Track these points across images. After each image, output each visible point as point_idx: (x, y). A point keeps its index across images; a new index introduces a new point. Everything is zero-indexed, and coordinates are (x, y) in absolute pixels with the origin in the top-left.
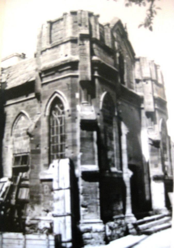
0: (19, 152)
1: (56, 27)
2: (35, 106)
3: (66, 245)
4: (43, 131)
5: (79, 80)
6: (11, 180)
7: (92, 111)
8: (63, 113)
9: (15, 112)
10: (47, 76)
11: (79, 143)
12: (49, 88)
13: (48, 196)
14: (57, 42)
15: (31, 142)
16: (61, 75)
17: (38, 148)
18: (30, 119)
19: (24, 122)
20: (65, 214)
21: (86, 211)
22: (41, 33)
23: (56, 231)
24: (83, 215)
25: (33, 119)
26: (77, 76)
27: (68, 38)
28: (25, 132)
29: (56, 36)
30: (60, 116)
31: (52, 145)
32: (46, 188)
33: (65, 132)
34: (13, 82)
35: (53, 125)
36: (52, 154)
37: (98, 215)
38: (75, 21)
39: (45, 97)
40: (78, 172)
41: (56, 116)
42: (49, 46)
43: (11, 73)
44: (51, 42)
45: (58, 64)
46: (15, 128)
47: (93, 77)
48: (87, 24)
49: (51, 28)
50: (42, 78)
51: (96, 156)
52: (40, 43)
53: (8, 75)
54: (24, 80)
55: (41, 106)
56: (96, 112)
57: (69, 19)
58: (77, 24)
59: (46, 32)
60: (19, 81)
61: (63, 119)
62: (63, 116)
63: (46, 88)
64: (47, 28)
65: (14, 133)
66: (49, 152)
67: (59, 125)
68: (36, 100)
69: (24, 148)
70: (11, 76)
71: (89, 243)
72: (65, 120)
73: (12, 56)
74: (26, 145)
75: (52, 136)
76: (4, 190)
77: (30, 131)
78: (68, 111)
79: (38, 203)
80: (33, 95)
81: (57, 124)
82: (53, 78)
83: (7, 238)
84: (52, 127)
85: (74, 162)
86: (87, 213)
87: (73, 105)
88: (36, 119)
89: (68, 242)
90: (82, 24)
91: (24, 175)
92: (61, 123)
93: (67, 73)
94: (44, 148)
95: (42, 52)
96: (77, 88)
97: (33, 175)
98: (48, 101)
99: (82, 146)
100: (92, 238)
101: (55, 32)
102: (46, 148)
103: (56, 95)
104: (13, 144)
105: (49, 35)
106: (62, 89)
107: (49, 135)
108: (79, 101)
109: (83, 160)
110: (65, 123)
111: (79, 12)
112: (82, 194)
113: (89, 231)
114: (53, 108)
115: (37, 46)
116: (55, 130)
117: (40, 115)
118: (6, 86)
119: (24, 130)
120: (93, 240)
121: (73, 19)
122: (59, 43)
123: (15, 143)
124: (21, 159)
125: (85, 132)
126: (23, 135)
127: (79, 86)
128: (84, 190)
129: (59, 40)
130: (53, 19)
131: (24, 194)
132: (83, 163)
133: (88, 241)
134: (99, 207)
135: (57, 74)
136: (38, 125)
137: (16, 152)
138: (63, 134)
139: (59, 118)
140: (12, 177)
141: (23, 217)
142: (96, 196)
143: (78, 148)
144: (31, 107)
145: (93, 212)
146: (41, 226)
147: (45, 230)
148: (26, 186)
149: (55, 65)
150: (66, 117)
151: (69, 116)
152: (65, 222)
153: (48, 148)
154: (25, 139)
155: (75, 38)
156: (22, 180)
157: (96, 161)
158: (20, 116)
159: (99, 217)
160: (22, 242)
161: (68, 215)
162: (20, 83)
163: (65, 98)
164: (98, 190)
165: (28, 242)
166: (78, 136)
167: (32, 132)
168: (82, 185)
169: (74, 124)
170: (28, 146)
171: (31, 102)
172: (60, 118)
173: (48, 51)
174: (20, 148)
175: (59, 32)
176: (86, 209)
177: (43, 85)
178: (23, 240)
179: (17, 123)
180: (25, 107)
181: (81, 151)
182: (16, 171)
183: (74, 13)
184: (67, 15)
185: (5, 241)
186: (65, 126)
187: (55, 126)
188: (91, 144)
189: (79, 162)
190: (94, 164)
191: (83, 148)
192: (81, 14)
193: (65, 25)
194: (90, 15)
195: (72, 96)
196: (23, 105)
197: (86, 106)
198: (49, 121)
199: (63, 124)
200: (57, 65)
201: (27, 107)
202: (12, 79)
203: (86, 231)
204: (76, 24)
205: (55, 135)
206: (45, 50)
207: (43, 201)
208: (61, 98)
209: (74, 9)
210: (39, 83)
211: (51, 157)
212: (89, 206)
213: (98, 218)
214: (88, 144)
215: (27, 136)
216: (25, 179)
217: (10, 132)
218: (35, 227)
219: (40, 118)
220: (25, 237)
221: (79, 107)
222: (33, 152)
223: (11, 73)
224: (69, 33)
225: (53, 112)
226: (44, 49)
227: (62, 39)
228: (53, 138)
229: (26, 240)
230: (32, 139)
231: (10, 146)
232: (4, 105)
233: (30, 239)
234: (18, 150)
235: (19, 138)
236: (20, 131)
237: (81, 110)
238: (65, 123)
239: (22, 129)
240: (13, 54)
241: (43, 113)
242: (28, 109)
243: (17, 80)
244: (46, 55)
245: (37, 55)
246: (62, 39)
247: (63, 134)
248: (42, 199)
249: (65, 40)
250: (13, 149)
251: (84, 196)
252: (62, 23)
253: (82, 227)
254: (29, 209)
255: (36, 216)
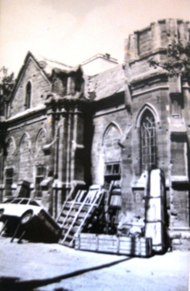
0: (111, 161)
1: (144, 38)
2: (125, 117)
3: (156, 249)
4: (134, 142)
5: (168, 92)
6: (103, 187)
7: (183, 123)
8: (154, 125)
9: (105, 122)
10: (136, 89)
11: (169, 155)
12: (139, 100)
13: (139, 203)
14: (146, 54)
15: (123, 153)
16: (151, 88)
17: (130, 159)
18: (120, 129)
19: (115, 132)
20: (156, 220)
21: (176, 219)
22: (129, 44)
23: (148, 235)
24: (173, 223)
25: (123, 130)
26: (167, 89)
27: (156, 50)
28: (116, 142)
29: (144, 47)
30: (151, 128)
31: (143, 155)
32: (138, 196)
33: (156, 143)
34: (101, 92)
35: (144, 136)
36: (143, 164)
37: (187, 223)
38: (164, 30)
39: (135, 110)
40: (168, 183)
41: (147, 128)
42: (138, 58)
43: (98, 82)
44: (139, 53)
45: (147, 77)
46: (106, 138)
47: (183, 89)
48: (176, 33)
49: (138, 39)
50: (131, 91)
51: (186, 167)
52: (128, 55)
53: (96, 84)
54: (113, 90)
55: (131, 118)
56: (186, 124)
57: (157, 30)
58: (166, 34)
59: (133, 42)
60: (108, 91)
61: (154, 131)
62: (153, 128)
63: (136, 100)
64: (134, 38)
65: (105, 144)
66: (141, 162)
67: (150, 137)
68: (126, 111)
69: (115, 158)
70: (99, 86)
71: (178, 249)
72: (155, 132)
73: (95, 57)
74: (117, 155)
75: (143, 147)
76: (98, 196)
77: (122, 142)
78: (159, 123)
79: (130, 209)
80: (123, 106)
81: (148, 135)
82: (142, 90)
83: (102, 239)
84: (143, 138)
85: (165, 173)
86: (176, 221)
87: (163, 117)
88: (127, 131)
89: (159, 245)
90: (171, 34)
91: (116, 183)
92: (152, 135)
93: (156, 86)
94: (135, 159)
95: (131, 64)
96: (167, 101)
97: (125, 184)
98: (139, 114)
99: (172, 157)
100: (181, 244)
101: (143, 43)
102: (137, 159)
103: (146, 107)
104: (104, 153)
105: (136, 46)
106: (152, 101)
107: (140, 146)
108: (169, 113)
109: (174, 170)
110: (155, 135)
111: (167, 21)
112: (172, 203)
113: (178, 237)
114: (143, 120)
115: (125, 58)
116: (146, 141)
117: (131, 127)
118: (95, 96)
119: (115, 140)
120: (182, 246)
121: (161, 29)
122: (148, 55)
123: (106, 152)
124: (112, 168)
125: (175, 143)
126: (115, 144)
127: (169, 99)
128: (174, 199)
129: (147, 52)
130: (140, 28)
131: (116, 201)
132: (173, 173)
133: (177, 246)
134: (188, 216)
135: (147, 86)
136: (129, 136)
137: (108, 161)
138: (154, 145)
139: (150, 130)
140: (104, 185)
141: (115, 222)
142: (186, 205)
143: (169, 159)
144: (122, 118)
145: (183, 220)
146: (132, 231)
147: (137, 234)
148: (119, 194)
149: (144, 78)
150: (157, 128)
151: (160, 128)
152: (155, 227)
153: (139, 158)
154: (117, 148)
155: (164, 50)
156: (114, 187)
157: (187, 172)
158: (110, 127)
159: (188, 224)
160: (116, 243)
161: (159, 221)
162: (108, 95)
163: (156, 110)
164: (188, 199)
165: (121, 243)
166: (168, 148)
167: (124, 143)
168: (172, 195)
169: (187, 249)
170: (120, 156)
171: (121, 113)
172: (151, 130)
173: (137, 64)
174: (111, 157)
175: (147, 43)
176: (176, 217)
177: (133, 97)
178: (118, 241)
179: (107, 134)
180: (115, 118)
181: (171, 162)
182: (108, 179)
183: (162, 22)
184: (155, 25)
185: (100, 242)
186: (155, 138)
187: (146, 138)
188: (181, 156)
189: (169, 173)
190: (184, 175)
191: (174, 159)
192: (169, 22)
193: (153, 36)
194: (180, 22)
195: (163, 109)
196: (113, 116)
197: (176, 118)
198: (140, 132)
199: (154, 136)
200: (146, 78)
201: (117, 118)
202: (101, 89)
203: (175, 237)
204: (164, 34)
205: (146, 146)
206: (134, 63)
207: (135, 208)
208: (152, 111)
209: (162, 18)
210: (128, 94)
211: (143, 167)
212: (179, 214)
213: (187, 226)
214: (178, 156)
215: (117, 146)
216: (118, 187)
217: (101, 142)
218: (127, 231)
219: (131, 130)
220: (119, 239)
221: (169, 120)
222: (125, 162)
223: (98, 82)
224: (157, 44)
225: (144, 124)
226: (133, 61)
227: (150, 51)
228: (144, 149)
229: (120, 241)
230: (124, 149)
231: (102, 155)
232: (93, 116)
233: (123, 241)
234: (110, 159)
235: (110, 148)
236: (112, 141)
237: (172, 123)
238: (155, 135)
239: (112, 139)
240: (96, 56)
241: (133, 125)
242: (119, 119)
243: (106, 89)
244: (135, 67)
245: (126, 68)
246: (150, 51)
247: (154, 145)
248: (133, 206)
249: (154, 52)
250: (105, 158)
251: (174, 204)
252: (150, 33)
253: (171, 234)
254: (121, 214)
255: (128, 221)
